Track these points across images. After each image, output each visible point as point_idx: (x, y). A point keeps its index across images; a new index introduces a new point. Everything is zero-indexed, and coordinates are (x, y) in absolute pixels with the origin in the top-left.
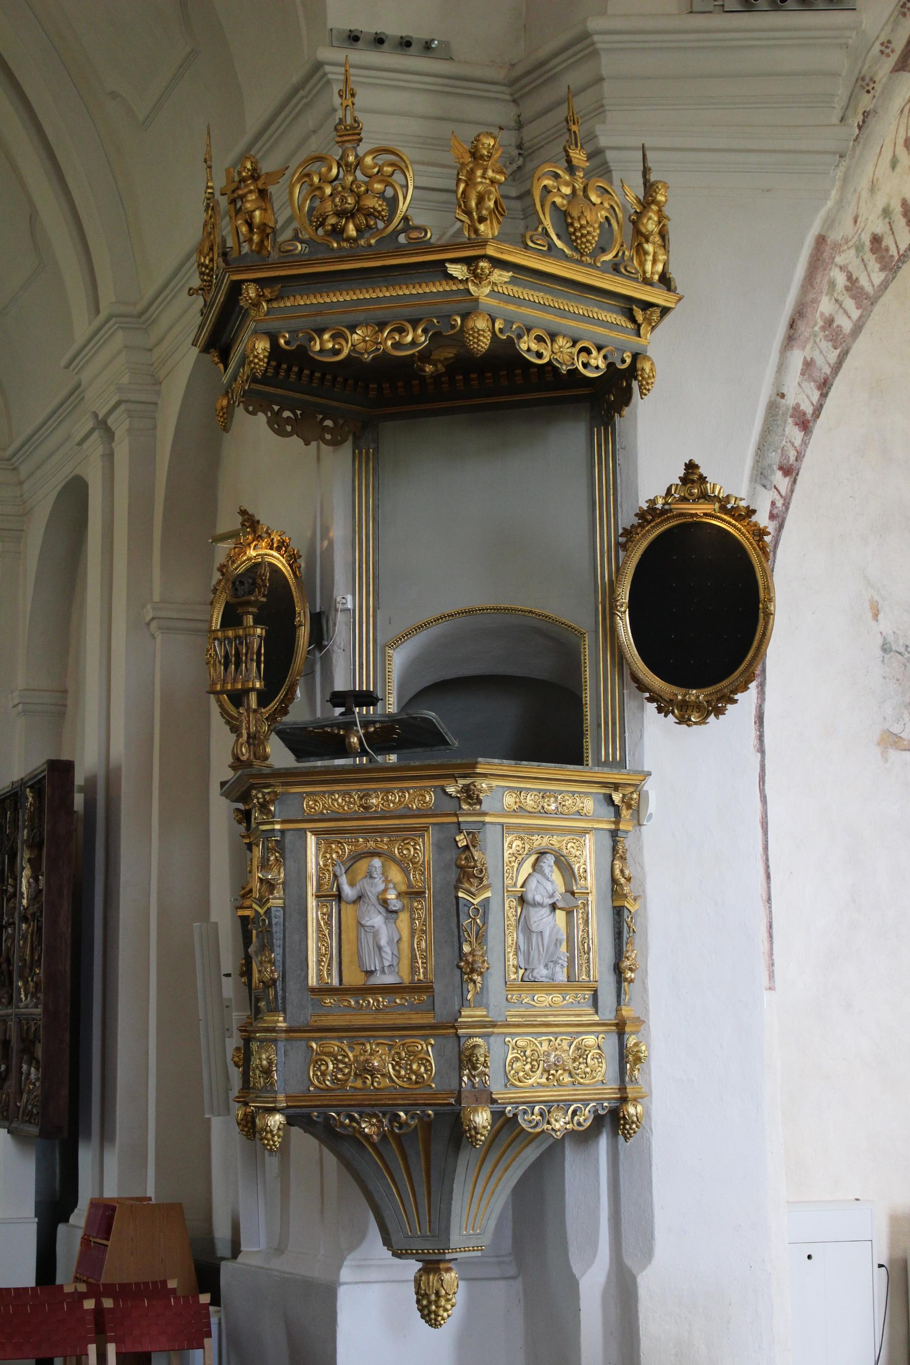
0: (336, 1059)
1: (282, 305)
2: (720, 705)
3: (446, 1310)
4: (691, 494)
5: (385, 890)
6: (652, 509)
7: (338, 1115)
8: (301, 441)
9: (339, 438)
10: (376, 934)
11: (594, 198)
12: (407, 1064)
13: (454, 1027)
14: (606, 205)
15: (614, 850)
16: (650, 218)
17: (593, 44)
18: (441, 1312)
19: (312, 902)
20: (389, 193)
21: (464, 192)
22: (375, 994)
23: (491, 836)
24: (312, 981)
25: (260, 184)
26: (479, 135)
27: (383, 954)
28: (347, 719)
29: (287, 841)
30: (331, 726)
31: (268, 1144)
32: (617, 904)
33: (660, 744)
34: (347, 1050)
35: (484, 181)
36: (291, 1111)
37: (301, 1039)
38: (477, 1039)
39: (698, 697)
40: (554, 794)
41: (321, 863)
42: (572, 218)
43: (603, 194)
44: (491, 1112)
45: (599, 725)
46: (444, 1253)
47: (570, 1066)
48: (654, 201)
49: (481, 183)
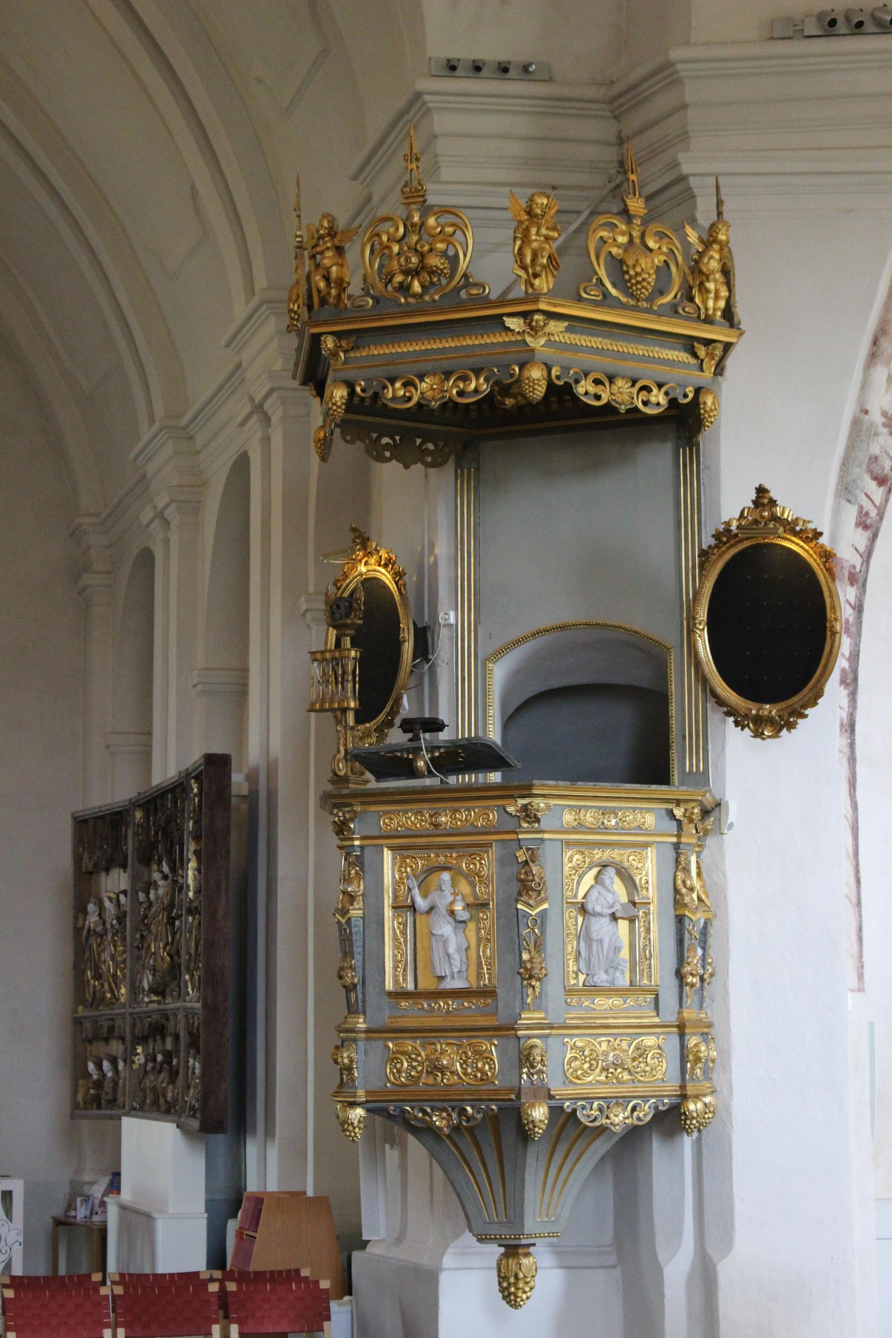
0: (410, 1058)
1: (358, 355)
2: (791, 720)
3: (525, 1292)
4: (762, 517)
5: (453, 902)
6: (728, 531)
7: (412, 1109)
8: (401, 466)
9: (440, 460)
10: (445, 943)
11: (651, 244)
12: (473, 1063)
13: (513, 1029)
14: (664, 249)
15: (677, 862)
16: (711, 257)
17: (676, 72)
18: (520, 1294)
19: (388, 913)
20: (451, 253)
21: (520, 249)
22: (445, 997)
23: (548, 853)
24: (389, 985)
25: (337, 241)
26: (533, 196)
27: (452, 962)
28: (415, 744)
29: (366, 855)
30: (402, 751)
31: (350, 1136)
32: (679, 912)
33: (741, 762)
34: (420, 1049)
35: (538, 238)
36: (371, 1105)
37: (379, 1039)
38: (536, 1040)
39: (770, 712)
40: (614, 812)
41: (397, 877)
42: (628, 266)
43: (661, 239)
44: (549, 1107)
45: (684, 737)
46: (520, 1239)
47: (629, 1064)
48: (715, 241)
49: (536, 240)
